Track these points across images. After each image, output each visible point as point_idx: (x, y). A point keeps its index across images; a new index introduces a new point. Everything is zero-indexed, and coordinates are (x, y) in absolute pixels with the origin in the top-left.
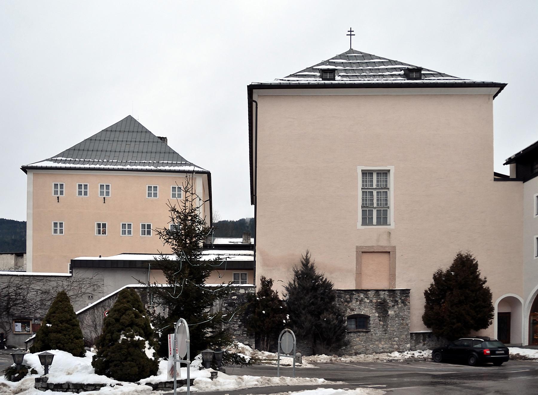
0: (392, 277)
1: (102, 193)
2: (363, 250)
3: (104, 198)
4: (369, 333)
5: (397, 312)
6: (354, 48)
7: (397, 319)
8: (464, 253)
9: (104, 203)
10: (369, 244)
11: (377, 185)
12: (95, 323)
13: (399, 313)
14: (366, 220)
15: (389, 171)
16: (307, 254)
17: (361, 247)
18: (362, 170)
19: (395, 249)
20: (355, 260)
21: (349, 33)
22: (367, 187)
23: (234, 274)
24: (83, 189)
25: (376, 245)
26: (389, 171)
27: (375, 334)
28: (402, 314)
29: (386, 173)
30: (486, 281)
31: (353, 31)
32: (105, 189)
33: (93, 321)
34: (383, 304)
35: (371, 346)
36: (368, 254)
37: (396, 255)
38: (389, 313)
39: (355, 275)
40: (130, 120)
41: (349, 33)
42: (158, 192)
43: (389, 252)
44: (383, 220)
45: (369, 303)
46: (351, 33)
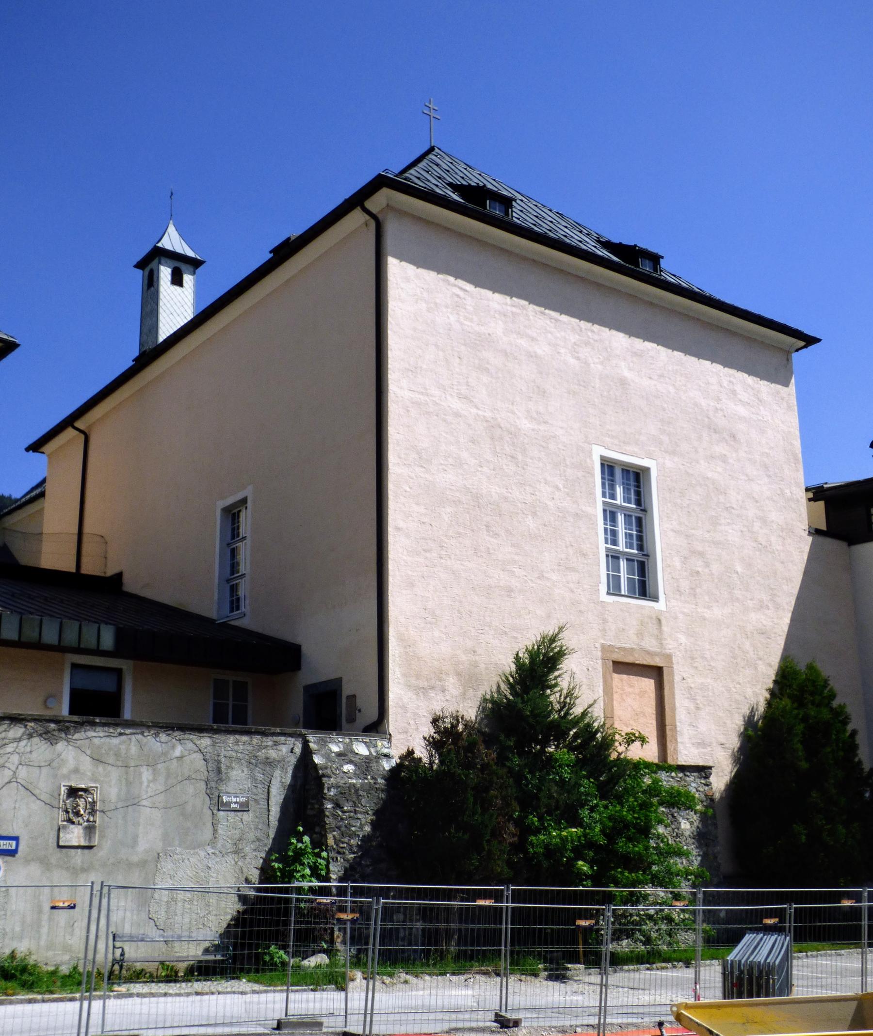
20: (601, 680)
23: (75, 666)
25: (658, 650)
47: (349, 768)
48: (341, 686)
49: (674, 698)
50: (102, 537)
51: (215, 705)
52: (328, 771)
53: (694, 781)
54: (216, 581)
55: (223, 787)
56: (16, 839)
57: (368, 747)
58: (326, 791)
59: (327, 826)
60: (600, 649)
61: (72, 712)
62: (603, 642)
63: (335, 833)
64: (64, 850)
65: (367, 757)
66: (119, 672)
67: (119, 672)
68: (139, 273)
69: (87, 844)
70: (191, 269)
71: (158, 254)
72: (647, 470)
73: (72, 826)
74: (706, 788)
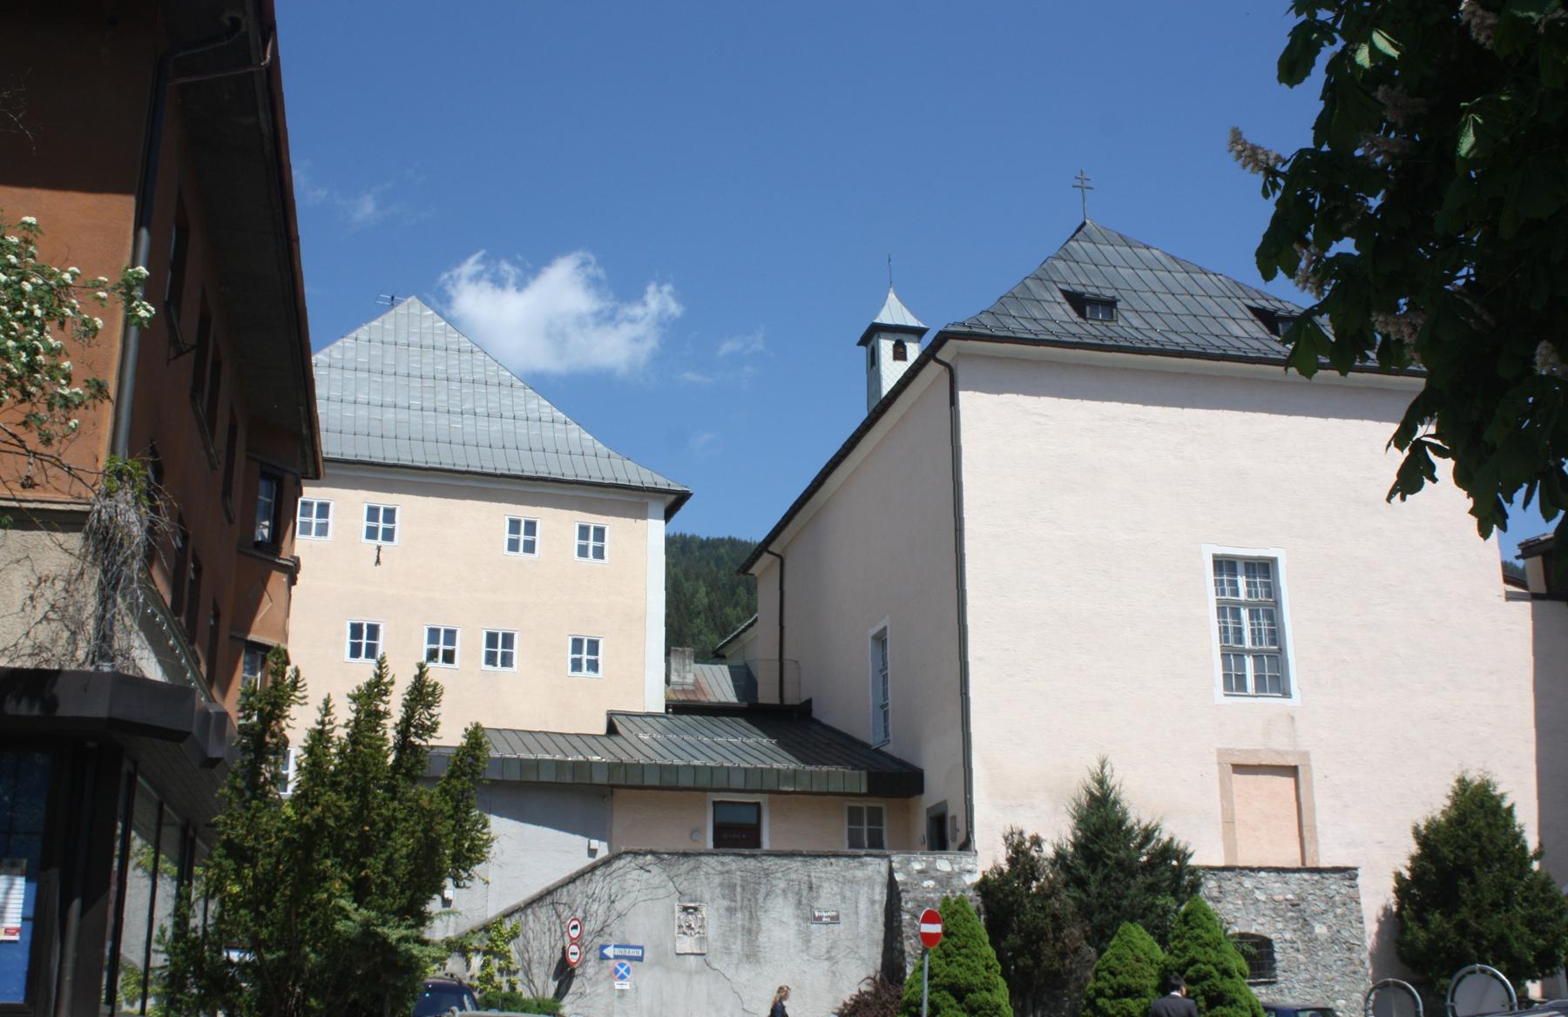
1: (372, 533)
3: (379, 548)
4: (1275, 987)
5: (1335, 928)
7: (1337, 948)
8: (1474, 776)
9: (378, 562)
12: (526, 956)
16: (1103, 767)
18: (1215, 556)
19: (1309, 760)
20: (1218, 785)
23: (715, 803)
25: (1292, 749)
27: (1289, 989)
30: (457, 886)
33: (522, 948)
34: (1298, 905)
39: (1220, 826)
47: (930, 883)
48: (946, 807)
49: (1313, 798)
50: (797, 662)
51: (850, 830)
52: (909, 888)
53: (1335, 883)
54: (871, 708)
55: (816, 905)
56: (641, 948)
57: (951, 863)
58: (903, 904)
59: (904, 935)
60: (1215, 753)
61: (716, 846)
62: (1220, 746)
63: (912, 941)
64: (681, 957)
65: (949, 873)
66: (758, 805)
67: (758, 805)
68: (863, 349)
69: (699, 952)
70: (915, 338)
71: (876, 331)
72: (1274, 561)
73: (686, 937)
74: (1351, 890)
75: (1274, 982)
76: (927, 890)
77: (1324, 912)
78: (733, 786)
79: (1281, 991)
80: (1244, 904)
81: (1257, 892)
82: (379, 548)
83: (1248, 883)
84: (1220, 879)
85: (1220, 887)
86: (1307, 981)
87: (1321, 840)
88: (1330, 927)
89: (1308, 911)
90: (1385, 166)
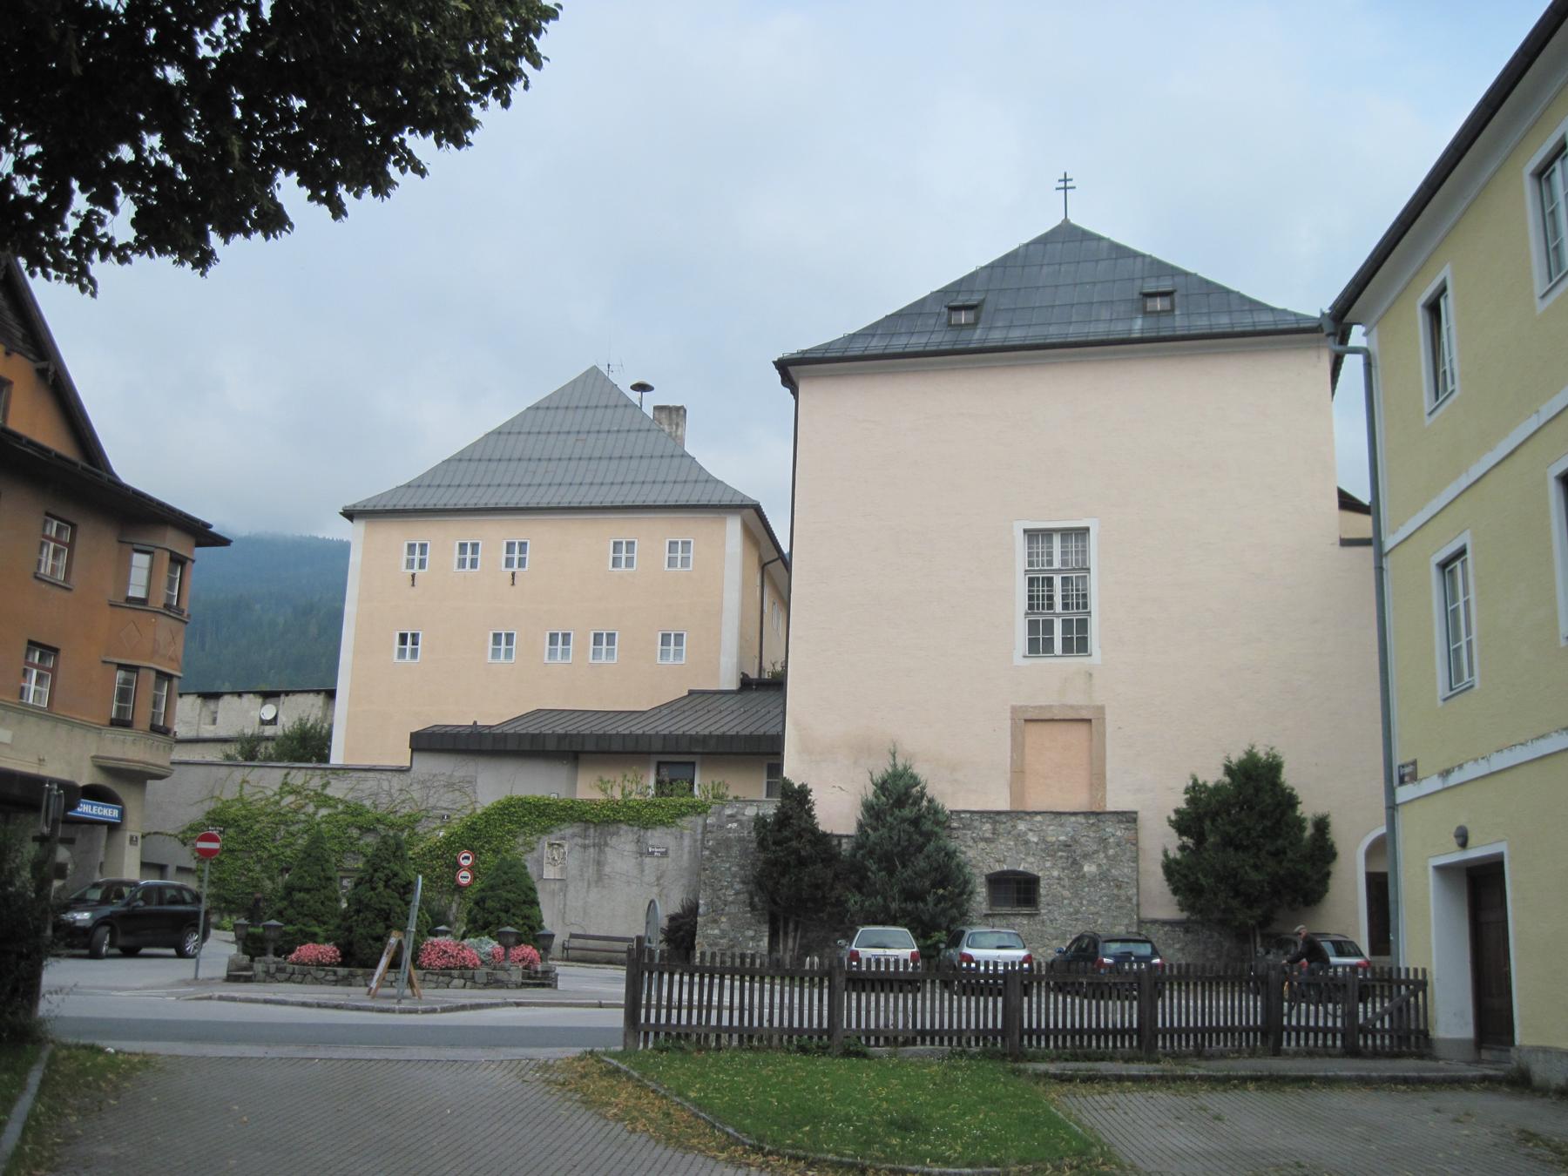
0: (1097, 779)
2: (1028, 716)
3: (513, 574)
4: (1037, 918)
5: (1105, 868)
6: (1073, 221)
10: (1042, 701)
11: (1064, 562)
13: (1108, 870)
14: (1039, 643)
15: (1087, 529)
17: (1024, 708)
19: (1104, 714)
21: (1062, 184)
22: (1041, 567)
24: (468, 553)
26: (1087, 529)
27: (1051, 921)
28: (1117, 873)
29: (1083, 532)
31: (1071, 180)
32: (516, 552)
34: (1070, 846)
35: (1040, 951)
36: (1040, 724)
37: (1104, 727)
38: (1086, 869)
40: (412, 734)
41: (1062, 184)
42: (635, 555)
43: (1089, 721)
44: (1077, 642)
45: (1037, 844)
46: (1065, 184)
51: (768, 783)
60: (1009, 711)
62: (1014, 703)
75: (1036, 914)
76: (730, 830)
77: (1096, 852)
78: (654, 749)
79: (1043, 922)
80: (1016, 845)
81: (1030, 834)
82: (513, 574)
83: (1022, 826)
84: (995, 822)
85: (994, 829)
86: (1071, 914)
87: (1109, 787)
88: (1099, 865)
89: (1078, 852)
90: (154, 56)
